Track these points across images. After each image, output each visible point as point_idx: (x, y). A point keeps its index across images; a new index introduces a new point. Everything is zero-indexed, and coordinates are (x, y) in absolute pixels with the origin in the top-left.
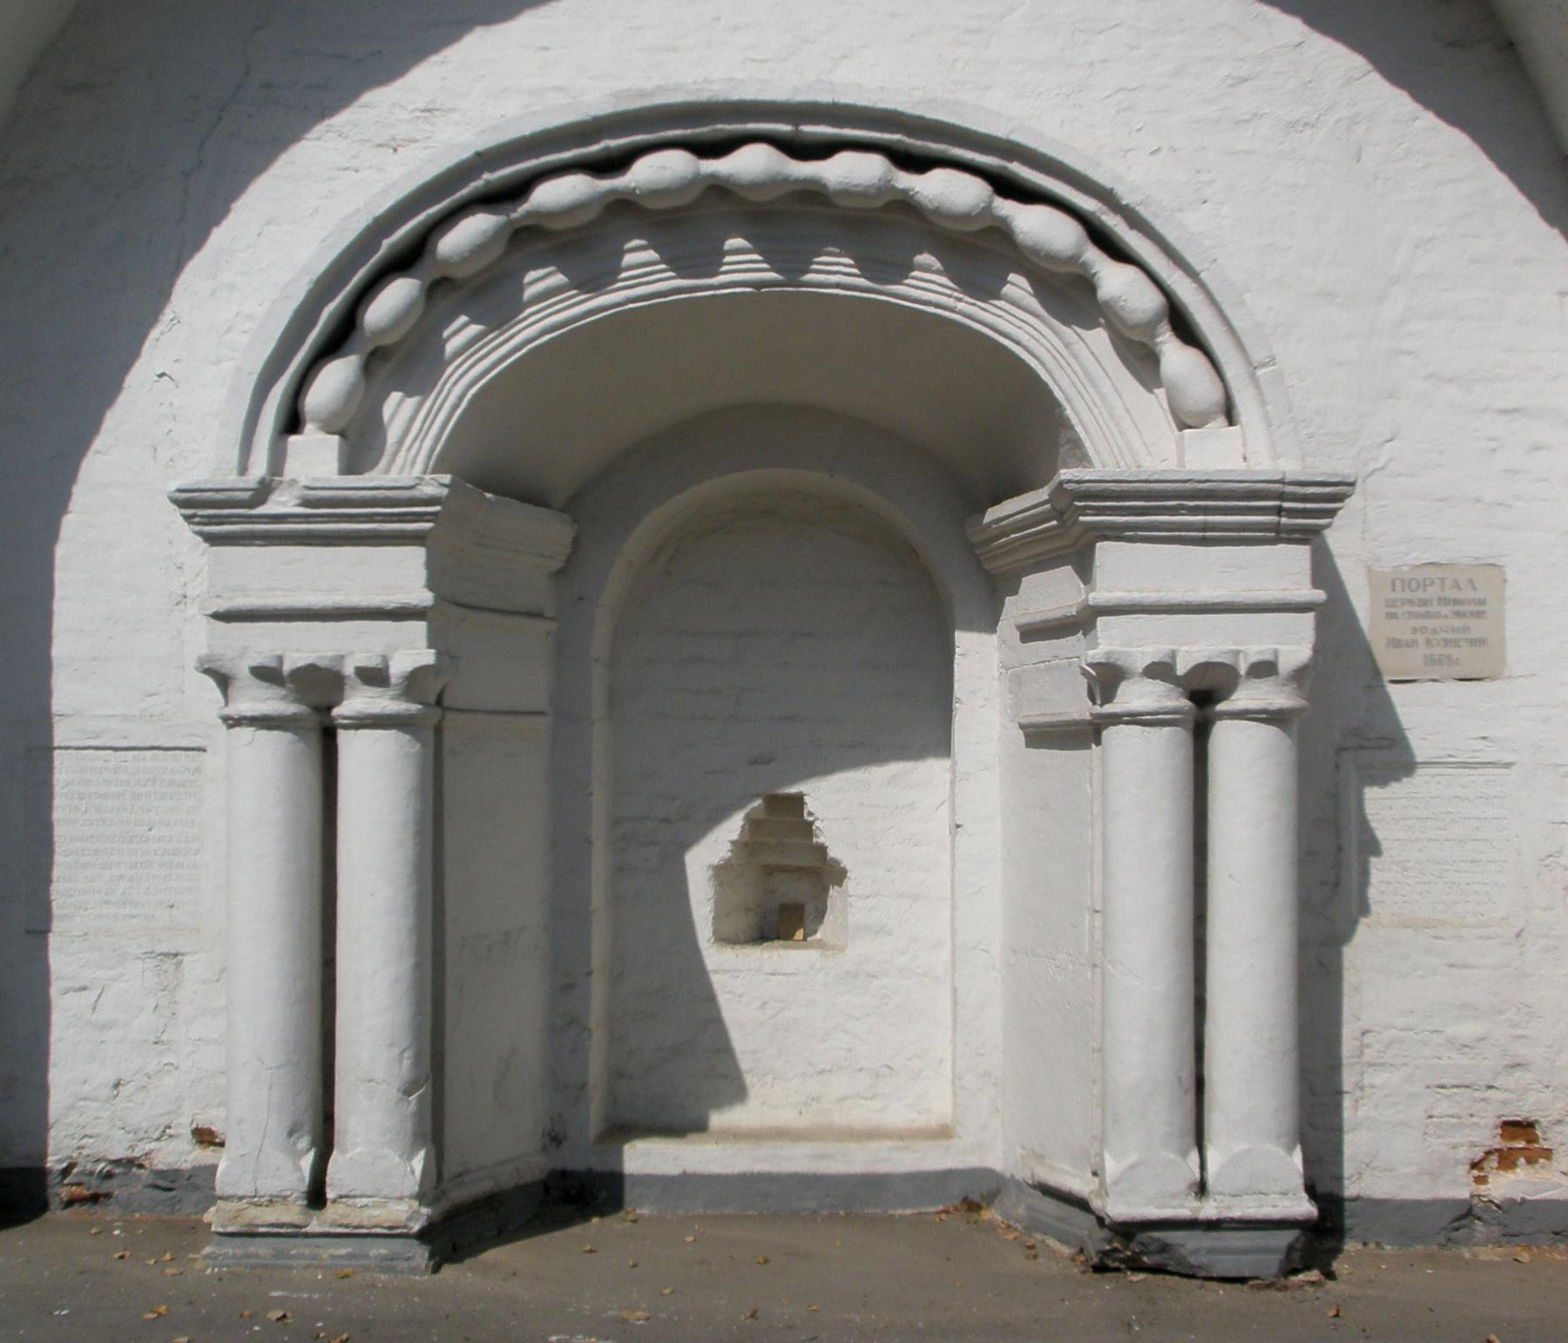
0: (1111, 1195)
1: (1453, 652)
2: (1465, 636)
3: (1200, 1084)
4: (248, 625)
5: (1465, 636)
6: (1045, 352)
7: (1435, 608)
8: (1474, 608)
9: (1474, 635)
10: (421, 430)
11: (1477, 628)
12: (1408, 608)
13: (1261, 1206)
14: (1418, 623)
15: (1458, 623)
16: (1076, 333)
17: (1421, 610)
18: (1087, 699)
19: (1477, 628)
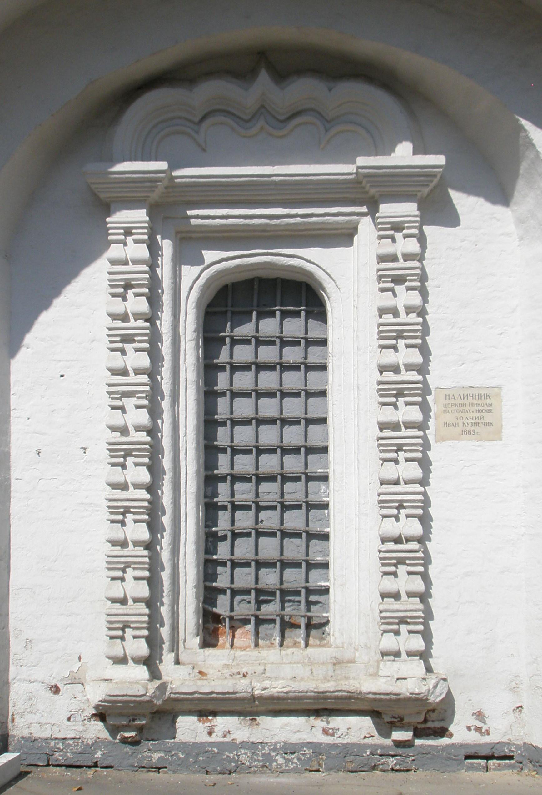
0: (111, 640)
1: (477, 429)
2: (482, 421)
3: (291, 236)
4: (307, 172)
5: (482, 421)
6: (197, 282)
7: (467, 408)
8: (486, 408)
9: (487, 420)
10: (404, 185)
11: (488, 418)
12: (454, 408)
13: (252, 707)
14: (459, 415)
15: (478, 415)
16: (162, 426)
17: (461, 409)
18: (82, 658)
19: (488, 418)
